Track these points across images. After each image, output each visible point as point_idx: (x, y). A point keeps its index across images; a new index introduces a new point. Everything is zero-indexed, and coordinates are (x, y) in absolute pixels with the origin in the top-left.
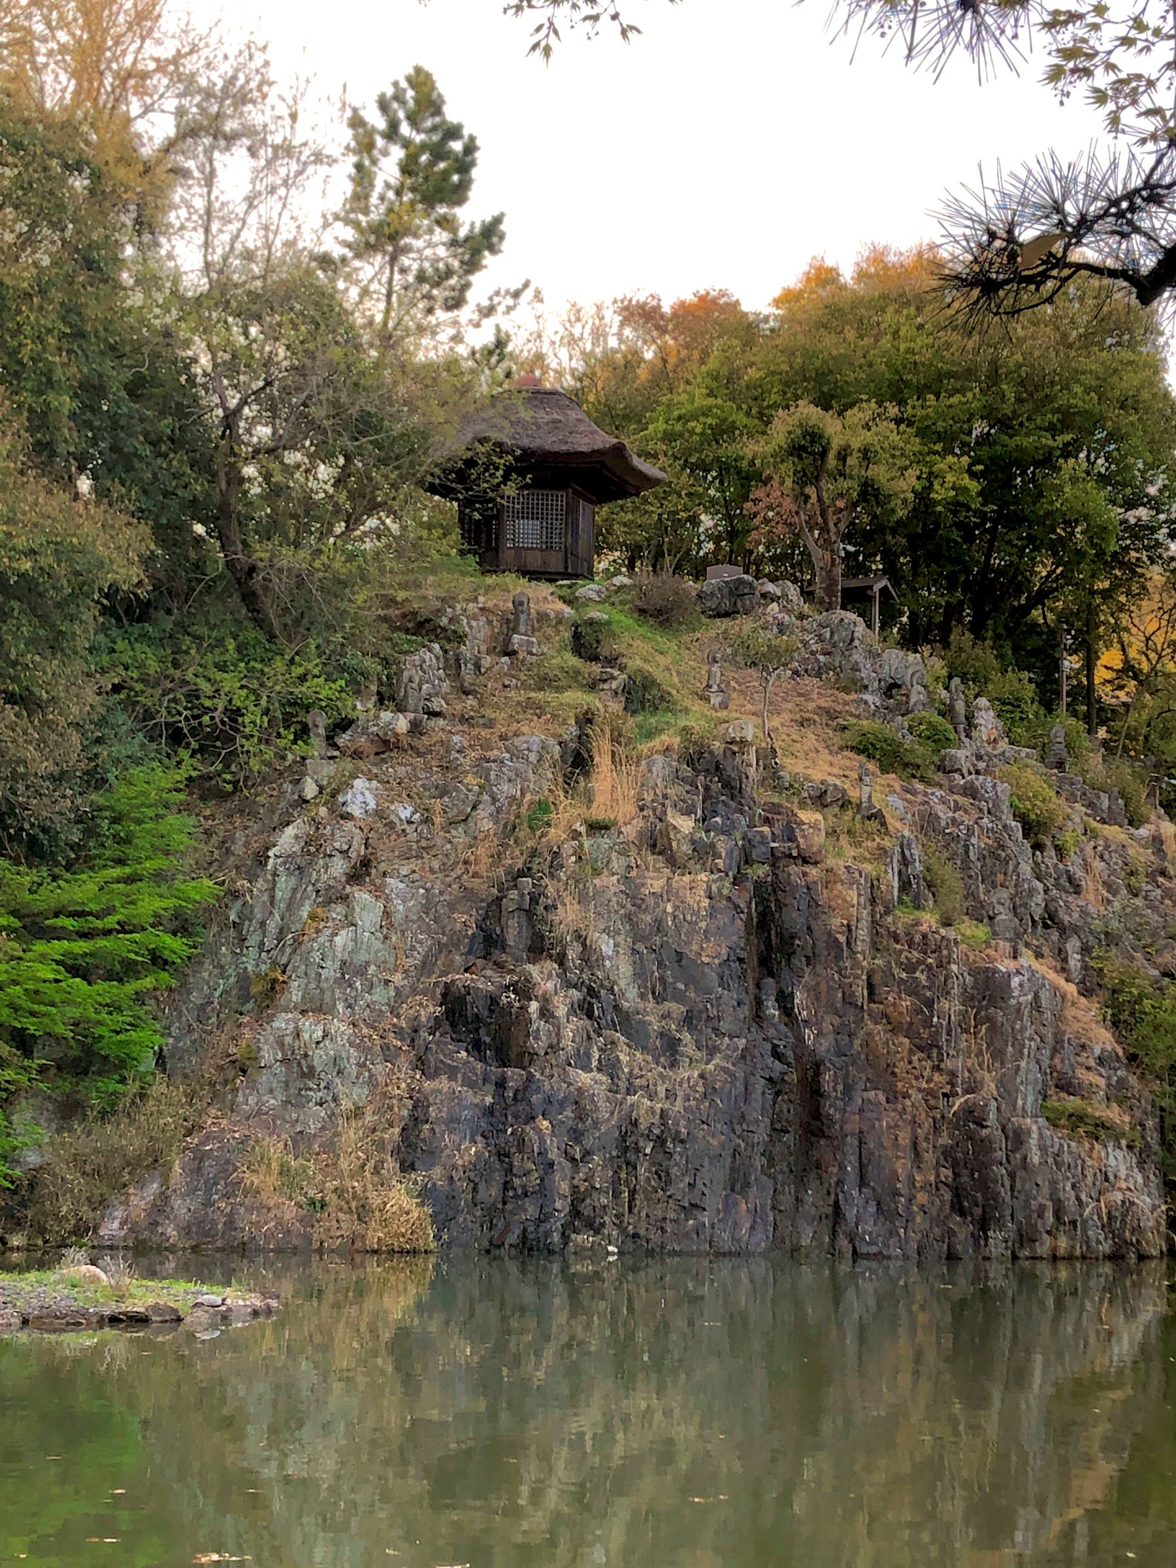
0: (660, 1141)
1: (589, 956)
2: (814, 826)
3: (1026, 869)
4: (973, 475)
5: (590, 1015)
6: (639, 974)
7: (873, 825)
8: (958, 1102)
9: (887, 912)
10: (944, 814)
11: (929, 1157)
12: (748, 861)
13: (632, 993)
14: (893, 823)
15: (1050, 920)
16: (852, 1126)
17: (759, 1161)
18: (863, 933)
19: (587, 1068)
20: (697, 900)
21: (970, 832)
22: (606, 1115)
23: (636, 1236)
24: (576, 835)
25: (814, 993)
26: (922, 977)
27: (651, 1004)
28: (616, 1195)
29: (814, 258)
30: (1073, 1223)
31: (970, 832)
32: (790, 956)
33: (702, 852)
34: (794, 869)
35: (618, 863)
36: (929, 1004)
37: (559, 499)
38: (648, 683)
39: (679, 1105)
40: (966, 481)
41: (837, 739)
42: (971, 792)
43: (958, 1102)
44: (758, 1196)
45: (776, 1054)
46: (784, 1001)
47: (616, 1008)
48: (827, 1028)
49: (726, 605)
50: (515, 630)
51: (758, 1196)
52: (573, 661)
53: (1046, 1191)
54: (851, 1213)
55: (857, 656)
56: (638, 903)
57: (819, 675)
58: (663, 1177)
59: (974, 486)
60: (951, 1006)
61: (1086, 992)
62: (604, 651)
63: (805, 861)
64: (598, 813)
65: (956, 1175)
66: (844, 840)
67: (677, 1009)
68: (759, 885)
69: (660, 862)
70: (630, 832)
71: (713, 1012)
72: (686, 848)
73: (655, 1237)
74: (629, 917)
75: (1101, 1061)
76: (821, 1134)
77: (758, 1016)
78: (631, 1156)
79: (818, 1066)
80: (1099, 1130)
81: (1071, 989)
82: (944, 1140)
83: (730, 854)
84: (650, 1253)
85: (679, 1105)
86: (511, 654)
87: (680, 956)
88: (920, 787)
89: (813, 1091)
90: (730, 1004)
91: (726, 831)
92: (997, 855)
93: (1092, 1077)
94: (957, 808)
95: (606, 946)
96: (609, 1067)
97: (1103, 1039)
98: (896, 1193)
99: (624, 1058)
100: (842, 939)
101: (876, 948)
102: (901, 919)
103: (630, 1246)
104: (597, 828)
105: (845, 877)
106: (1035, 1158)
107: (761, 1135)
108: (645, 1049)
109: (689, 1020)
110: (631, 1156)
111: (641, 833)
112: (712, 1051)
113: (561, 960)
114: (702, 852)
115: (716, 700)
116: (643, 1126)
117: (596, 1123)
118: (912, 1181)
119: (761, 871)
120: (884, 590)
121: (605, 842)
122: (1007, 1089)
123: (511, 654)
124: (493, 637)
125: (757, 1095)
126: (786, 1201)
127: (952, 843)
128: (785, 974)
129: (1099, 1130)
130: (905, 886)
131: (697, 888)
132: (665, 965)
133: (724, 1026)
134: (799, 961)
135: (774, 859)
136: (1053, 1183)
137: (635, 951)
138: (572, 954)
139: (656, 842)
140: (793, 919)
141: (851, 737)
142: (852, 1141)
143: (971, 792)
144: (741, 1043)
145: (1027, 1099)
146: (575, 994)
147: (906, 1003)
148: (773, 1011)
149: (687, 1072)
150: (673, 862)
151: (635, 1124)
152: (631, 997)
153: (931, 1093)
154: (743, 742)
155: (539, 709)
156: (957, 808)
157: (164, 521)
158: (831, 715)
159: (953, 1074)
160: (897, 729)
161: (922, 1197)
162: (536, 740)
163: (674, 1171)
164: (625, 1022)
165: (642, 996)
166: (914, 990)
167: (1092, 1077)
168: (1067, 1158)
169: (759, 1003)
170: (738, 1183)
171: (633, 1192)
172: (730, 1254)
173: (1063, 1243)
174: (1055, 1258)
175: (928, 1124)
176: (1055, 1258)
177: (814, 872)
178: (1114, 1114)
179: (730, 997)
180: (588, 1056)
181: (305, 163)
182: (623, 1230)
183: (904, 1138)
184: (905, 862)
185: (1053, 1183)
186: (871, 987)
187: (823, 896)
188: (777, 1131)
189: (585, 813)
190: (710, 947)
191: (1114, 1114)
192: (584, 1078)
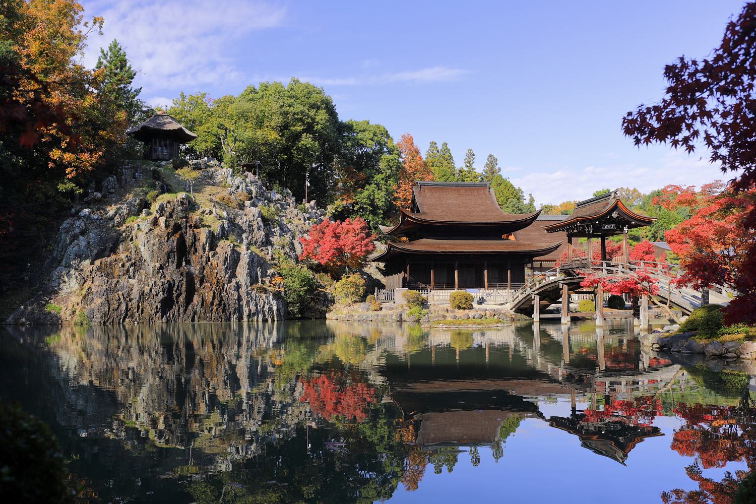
86: (135, 178)
123: (135, 178)
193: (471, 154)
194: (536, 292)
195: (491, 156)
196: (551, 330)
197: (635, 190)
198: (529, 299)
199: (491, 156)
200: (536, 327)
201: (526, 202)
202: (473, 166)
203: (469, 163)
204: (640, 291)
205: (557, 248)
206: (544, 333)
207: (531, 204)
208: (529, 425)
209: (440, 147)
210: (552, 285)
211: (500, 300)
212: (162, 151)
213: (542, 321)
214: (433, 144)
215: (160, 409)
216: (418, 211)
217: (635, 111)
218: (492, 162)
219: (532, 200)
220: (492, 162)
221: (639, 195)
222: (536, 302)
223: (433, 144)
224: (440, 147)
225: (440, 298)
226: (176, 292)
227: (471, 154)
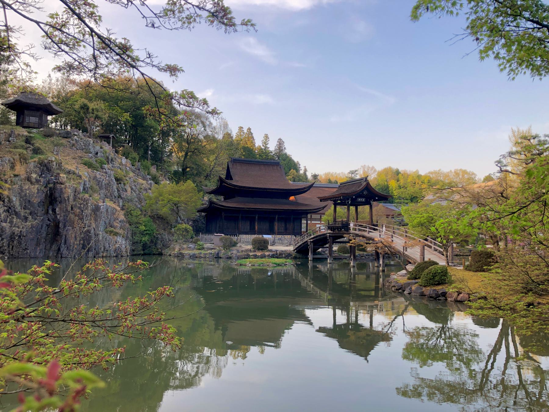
0: (20, 237)
1: (10, 201)
2: (64, 177)
3: (115, 187)
4: (130, 117)
5: (9, 212)
6: (21, 205)
7: (78, 178)
8: (85, 229)
9: (79, 194)
10: (98, 176)
11: (78, 239)
12: (49, 184)
13: (19, 208)
14: (83, 177)
15: (120, 196)
16: (65, 233)
17: (43, 240)
18: (71, 198)
19: (6, 222)
20: (35, 191)
21: (103, 180)
22: (8, 231)
23: (12, 255)
24: (11, 177)
25: (60, 209)
26: (82, 206)
27: (23, 210)
28: (9, 247)
29: (215, 108)
30: (107, 250)
31: (103, 180)
32: (56, 201)
33: (38, 181)
34: (58, 185)
35: (19, 183)
36: (82, 211)
37: (38, 113)
38: (39, 149)
39: (25, 230)
40: (129, 118)
41: (80, 161)
42: (106, 173)
43: (85, 229)
44: (42, 246)
45: (49, 220)
46: (54, 210)
47: (15, 211)
48: (62, 215)
49: (65, 136)
50: (10, 137)
51: (42, 246)
52: (24, 144)
53: (102, 245)
54: (62, 250)
55: (90, 147)
56: (22, 190)
57: (82, 150)
58: (20, 243)
59: (130, 119)
60: (88, 212)
61: (122, 209)
62: (32, 142)
63: (61, 184)
64: (16, 173)
65: (84, 242)
66: (72, 180)
67: (28, 211)
68: (50, 188)
69: (29, 183)
70: (23, 177)
71: (36, 212)
72: (34, 180)
73: (17, 255)
74: (19, 193)
75: (120, 222)
76: (58, 235)
77: (47, 212)
78: (13, 239)
79: (59, 222)
80: (116, 234)
81: (119, 209)
82: (82, 236)
83: (44, 182)
84: (15, 258)
85: (25, 230)
86: (9, 141)
87: (29, 201)
88: (95, 171)
89: (57, 226)
90: (40, 211)
91: (44, 178)
92: (108, 185)
93: (118, 225)
94: (102, 175)
95: (14, 199)
96: (11, 222)
97: (122, 217)
98: (71, 246)
99: (14, 220)
100: (66, 199)
101: (74, 200)
102: (81, 196)
103: (11, 256)
104: (16, 176)
105: (69, 187)
106: (101, 238)
107: (44, 235)
108: (20, 219)
109: (31, 214)
110: (13, 239)
111: (26, 177)
112: (35, 219)
113: (4, 201)
114: (38, 181)
115: (55, 153)
116: (16, 234)
117: (5, 233)
118: (74, 243)
119: (51, 185)
120: (113, 137)
121: (17, 179)
122: (97, 226)
123: (9, 141)
124: (6, 138)
125: (44, 228)
126: (48, 247)
127: (99, 183)
128: (55, 205)
129: (116, 234)
130: (84, 189)
131: (35, 188)
132: (27, 203)
133: (38, 215)
134: (58, 203)
135: (54, 183)
136: (104, 244)
137: (20, 200)
138: (6, 200)
139: (29, 179)
140: (57, 195)
141: (83, 162)
142: (64, 236)
143: (106, 173)
144: (42, 218)
145: (102, 228)
146: (6, 208)
147: (78, 211)
148: (50, 212)
149: (28, 224)
150: (32, 183)
151: (14, 233)
152: (18, 209)
153: (81, 227)
154: (52, 161)
155: (11, 152)
156: (102, 175)
157: (173, 154)
158: (81, 157)
159: (85, 224)
160: (93, 161)
161: (76, 246)
162: (8, 158)
163: (22, 242)
164: (17, 214)
165: (21, 209)
166: (80, 208)
167: (118, 225)
168: (108, 239)
169: (48, 210)
170: (38, 244)
171: (13, 247)
172: (33, 258)
173: (105, 255)
174: (103, 257)
175: (79, 233)
176: (103, 257)
177: (63, 186)
178: (121, 231)
179: (40, 209)
180: (7, 220)
182: (9, 253)
183: (73, 236)
184: (85, 184)
185: (104, 244)
186: (72, 208)
187: (64, 190)
188: (47, 235)
189: (14, 173)
190: (36, 200)
191: (121, 231)
192: (4, 224)
193: (266, 137)
194: (312, 240)
195: (280, 139)
196: (321, 267)
197: (373, 167)
198: (305, 245)
199: (280, 139)
200: (310, 264)
201: (302, 172)
202: (268, 146)
203: (265, 143)
205: (326, 206)
206: (315, 267)
207: (305, 173)
208: (298, 326)
209: (245, 131)
210: (322, 237)
211: (285, 244)
212: (33, 120)
213: (314, 260)
214: (241, 128)
215: (108, 72)
216: (232, 179)
217: (232, 15)
218: (281, 143)
219: (305, 171)
220: (281, 143)
221: (375, 171)
222: (311, 247)
223: (241, 128)
224: (245, 131)
225: (245, 242)
226: (18, 279)
227: (266, 137)
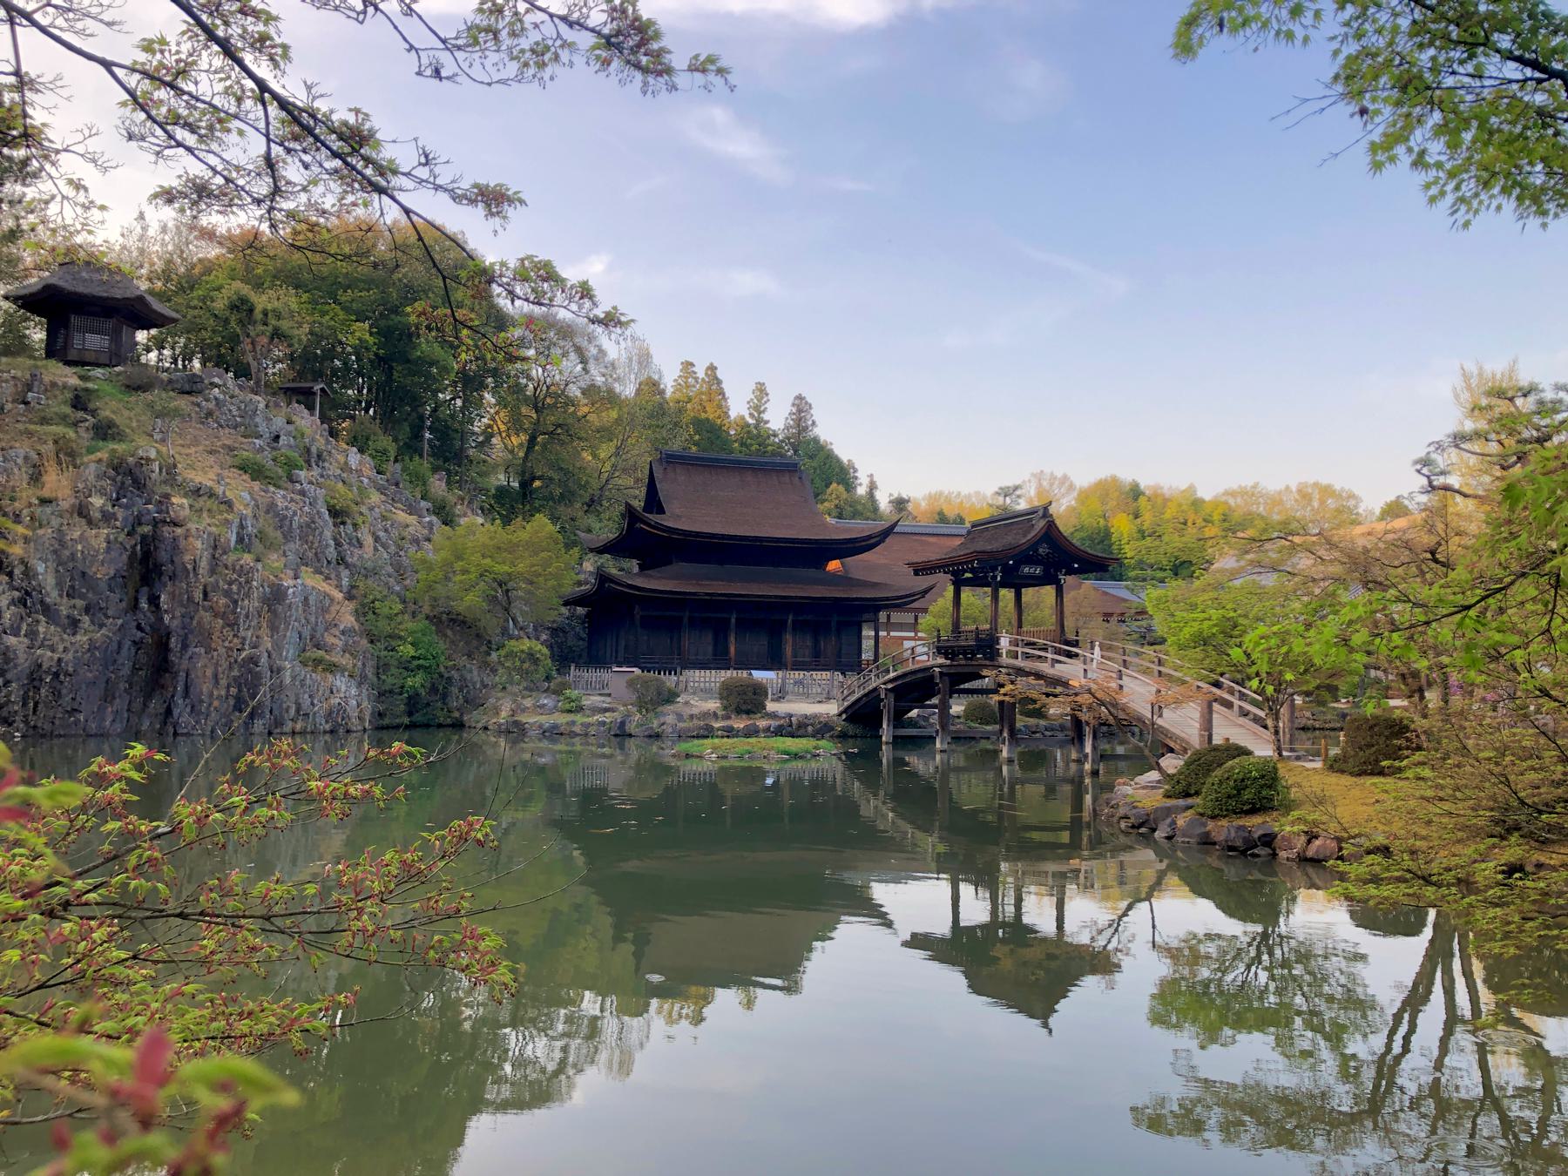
0: (56, 675)
1: (28, 573)
2: (181, 506)
3: (328, 534)
4: (371, 334)
5: (25, 605)
6: (59, 584)
7: (223, 507)
8: (244, 654)
9: (225, 553)
10: (281, 503)
11: (223, 682)
12: (140, 524)
13: (55, 594)
14: (238, 506)
15: (341, 561)
16: (185, 664)
17: (123, 686)
18: (204, 564)
19: (16, 635)
20: (100, 546)
21: (295, 513)
22: (23, 661)
23: (35, 727)
24: (30, 505)
25: (173, 596)
26: (234, 587)
27: (65, 599)
28: (25, 704)
30: (307, 715)
31: (295, 513)
32: (161, 574)
33: (107, 517)
34: (166, 529)
35: (55, 522)
36: (235, 602)
37: (110, 324)
38: (111, 425)
39: (70, 656)
40: (367, 336)
41: (229, 461)
42: (303, 493)
43: (244, 654)
44: (120, 704)
45: (139, 627)
46: (154, 601)
47: (42, 602)
48: (178, 614)
49: (187, 387)
50: (30, 390)
51: (120, 704)
52: (68, 410)
53: (293, 698)
54: (176, 712)
55: (257, 420)
56: (62, 543)
57: (235, 428)
58: (56, 694)
59: (371, 340)
60: (253, 604)
61: (350, 597)
62: (91, 406)
63: (176, 525)
64: (46, 493)
65: (240, 691)
66: (205, 515)
67: (80, 603)
68: (144, 537)
69: (83, 521)
70: (65, 505)
71: (103, 605)
72: (98, 515)
73: (48, 727)
74: (55, 552)
75: (343, 633)
76: (167, 670)
77: (135, 606)
78: (36, 683)
79: (168, 635)
80: (332, 668)
81: (339, 596)
82: (236, 673)
83: (125, 519)
84: (43, 736)
85: (70, 656)
86: (26, 403)
87: (84, 574)
88: (272, 489)
89: (163, 646)
90: (115, 601)
91: (126, 507)
92: (310, 527)
93: (336, 641)
94: (292, 500)
95: (41, 568)
96: (32, 634)
97: (348, 620)
98: (202, 701)
99: (41, 629)
100: (189, 567)
101: (212, 572)
102: (230, 558)
103: (31, 732)
104: (44, 501)
105: (197, 532)
106: (288, 680)
107: (126, 671)
108: (57, 625)
109: (87, 610)
110: (36, 683)
111: (73, 506)
112: (101, 626)
113: (10, 574)
114: (107, 517)
115: (157, 437)
116: (45, 667)
117: (16, 666)
118: (211, 695)
119: (146, 529)
120: (322, 390)
121: (48, 510)
122: (278, 646)
123: (26, 403)
124: (17, 393)
125: (124, 651)
126: (137, 705)
127: (282, 521)
128: (157, 584)
129: (332, 668)
130: (240, 540)
131: (99, 538)
132: (76, 578)
133: (110, 613)
134: (165, 579)
135: (155, 523)
136: (297, 695)
137: (57, 571)
138: (17, 572)
139: (82, 511)
140: (163, 556)
141: (237, 462)
142: (183, 674)
143: (303, 493)
144: (120, 622)
145: (290, 651)
146: (16, 594)
147: (223, 601)
148: (144, 605)
149: (81, 638)
150: (90, 522)
151: (40, 666)
152: (52, 596)
153: (231, 649)
154: (148, 459)
155: (30, 434)
156: (292, 500)
158: (231, 449)
159: (244, 639)
160: (266, 459)
161: (216, 703)
162: (22, 452)
163: (64, 691)
164: (47, 610)
165: (61, 596)
166: (227, 594)
167: (336, 641)
168: (308, 682)
169: (136, 599)
170: (108, 697)
171: (36, 704)
172: (96, 735)
173: (298, 727)
174: (294, 733)
175: (225, 665)
176: (294, 733)
177: (179, 531)
178: (345, 661)
179: (115, 597)
180: (19, 628)
181: (304, 189)
182: (26, 722)
183: (209, 673)
184: (242, 526)
185: (297, 695)
186: (205, 594)
187: (182, 543)
188: (135, 669)
189: (40, 493)
190: (103, 570)
191: (345, 661)
192: (11, 640)
193: (761, 390)
194: (890, 686)
195: (800, 398)
196: (915, 762)
197: (1065, 478)
198: (872, 699)
199: (800, 398)
200: (886, 754)
201: (861, 491)
202: (765, 417)
203: (758, 409)
204: (1498, 1021)
205: (930, 589)
206: (898, 762)
207: (871, 494)
208: (851, 932)
209: (701, 374)
210: (920, 675)
211: (813, 697)
212: (95, 342)
213: (898, 742)
214: (688, 365)
215: (309, 204)
216: (661, 511)
218: (801, 408)
219: (873, 487)
220: (801, 408)
221: (1071, 487)
222: (888, 704)
223: (688, 365)
224: (701, 374)
225: (700, 691)
226: (51, 796)
227: (761, 390)
